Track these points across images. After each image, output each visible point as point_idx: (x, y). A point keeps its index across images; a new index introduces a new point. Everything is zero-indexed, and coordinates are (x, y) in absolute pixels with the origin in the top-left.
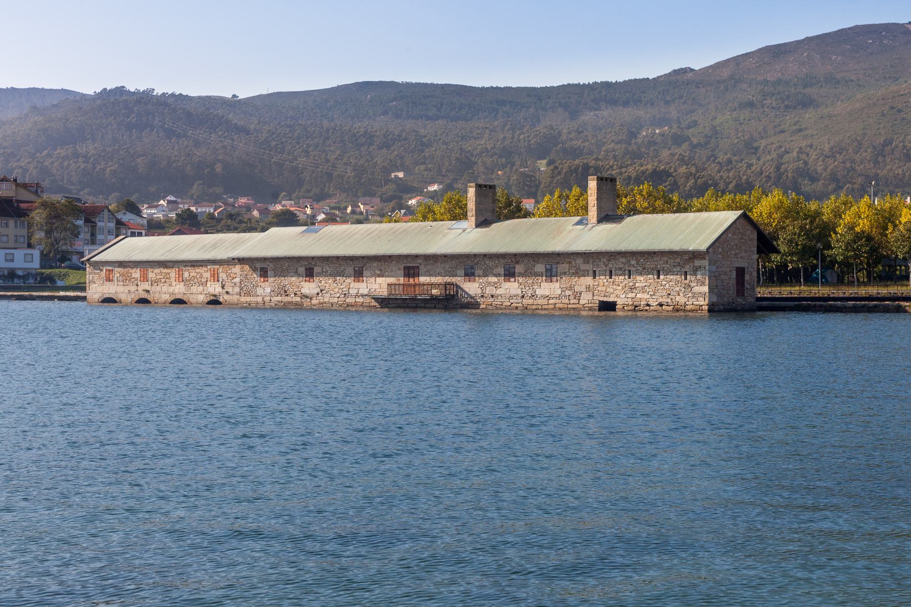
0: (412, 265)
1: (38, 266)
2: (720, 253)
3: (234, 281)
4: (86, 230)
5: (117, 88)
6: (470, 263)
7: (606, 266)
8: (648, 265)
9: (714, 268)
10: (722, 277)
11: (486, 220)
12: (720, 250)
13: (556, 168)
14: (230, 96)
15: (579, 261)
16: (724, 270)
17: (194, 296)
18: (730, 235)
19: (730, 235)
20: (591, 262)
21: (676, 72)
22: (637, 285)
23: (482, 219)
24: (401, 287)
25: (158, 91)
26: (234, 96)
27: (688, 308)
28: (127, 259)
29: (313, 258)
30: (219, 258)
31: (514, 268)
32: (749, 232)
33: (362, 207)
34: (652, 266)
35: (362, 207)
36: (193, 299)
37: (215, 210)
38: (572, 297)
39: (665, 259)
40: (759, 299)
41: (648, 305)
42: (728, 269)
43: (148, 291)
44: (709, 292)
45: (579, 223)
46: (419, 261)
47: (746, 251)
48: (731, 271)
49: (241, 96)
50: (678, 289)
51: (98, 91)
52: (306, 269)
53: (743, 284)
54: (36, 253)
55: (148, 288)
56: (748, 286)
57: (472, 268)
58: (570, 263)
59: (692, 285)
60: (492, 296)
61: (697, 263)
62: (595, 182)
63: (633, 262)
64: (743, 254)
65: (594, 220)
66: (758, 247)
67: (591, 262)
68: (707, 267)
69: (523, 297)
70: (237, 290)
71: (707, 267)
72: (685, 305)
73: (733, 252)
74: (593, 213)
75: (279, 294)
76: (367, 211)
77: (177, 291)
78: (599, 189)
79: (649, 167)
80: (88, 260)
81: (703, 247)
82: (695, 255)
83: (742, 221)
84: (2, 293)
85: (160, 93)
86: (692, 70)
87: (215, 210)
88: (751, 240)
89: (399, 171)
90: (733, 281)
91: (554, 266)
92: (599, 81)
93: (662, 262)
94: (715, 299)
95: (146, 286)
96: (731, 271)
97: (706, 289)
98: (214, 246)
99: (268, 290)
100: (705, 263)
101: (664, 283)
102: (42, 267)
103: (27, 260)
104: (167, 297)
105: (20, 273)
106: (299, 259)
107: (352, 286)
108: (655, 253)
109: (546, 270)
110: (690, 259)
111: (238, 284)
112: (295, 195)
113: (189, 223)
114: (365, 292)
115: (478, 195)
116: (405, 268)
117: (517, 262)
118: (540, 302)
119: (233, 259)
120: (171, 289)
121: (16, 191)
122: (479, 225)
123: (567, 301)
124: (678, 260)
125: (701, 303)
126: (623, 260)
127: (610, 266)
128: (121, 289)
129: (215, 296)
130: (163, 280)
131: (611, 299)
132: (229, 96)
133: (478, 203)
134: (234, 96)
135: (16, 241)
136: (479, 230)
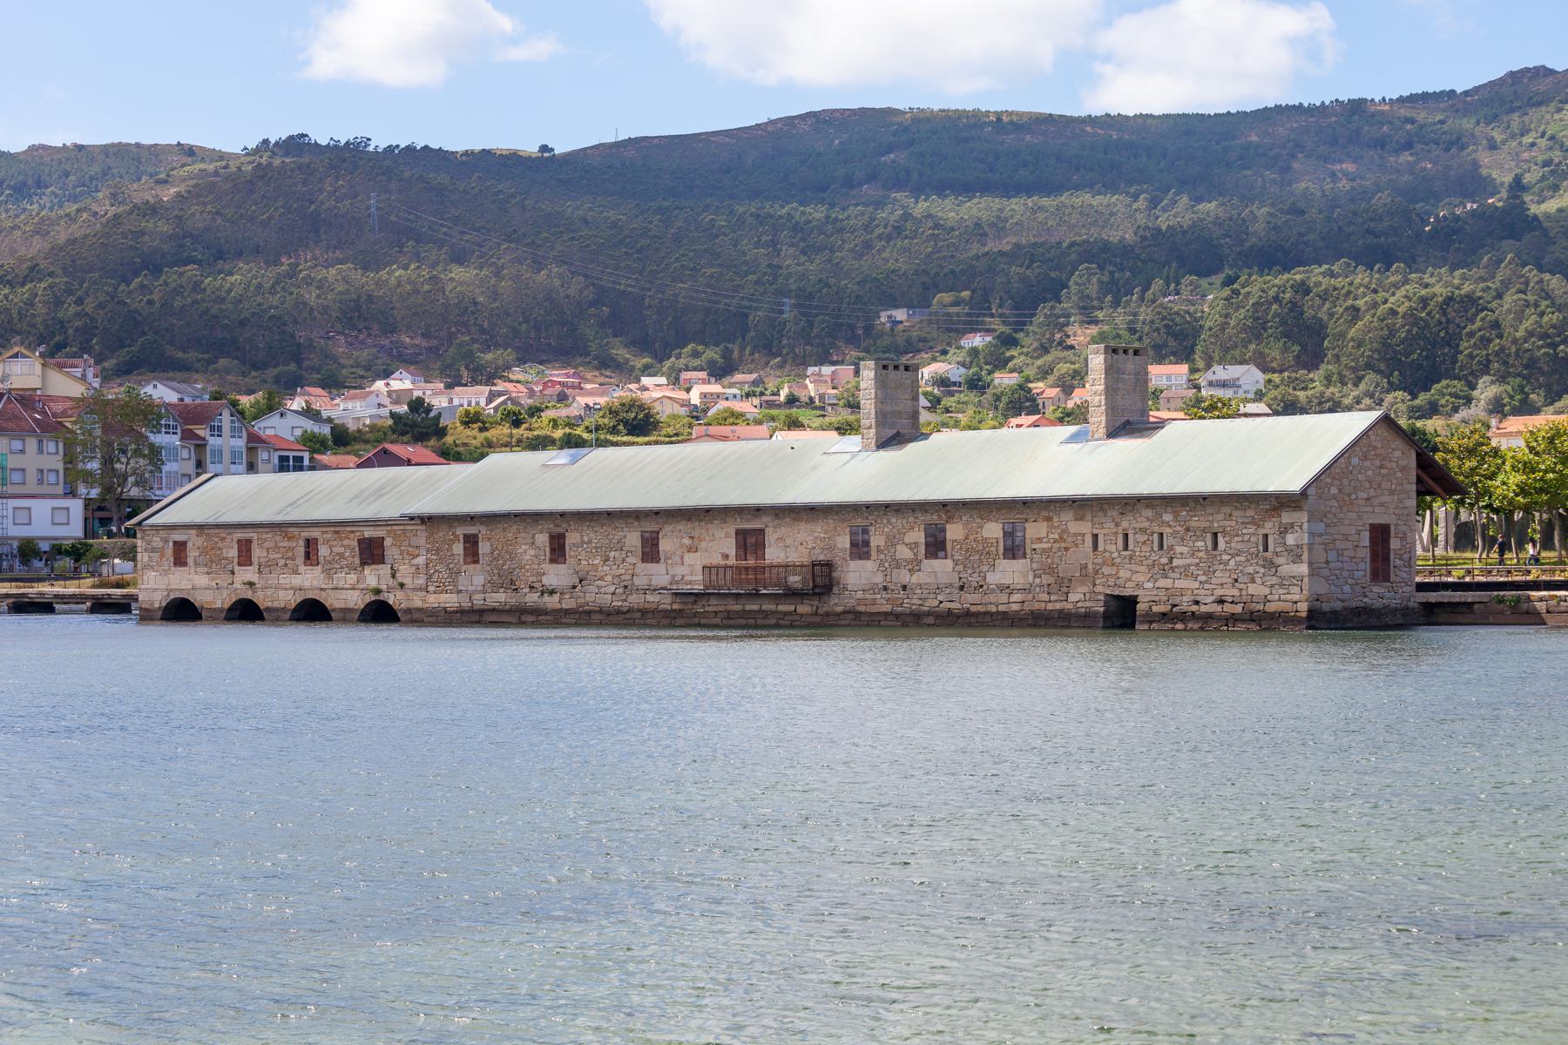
1: (79, 533)
3: (415, 561)
4: (185, 454)
5: (291, 138)
7: (1117, 525)
9: (1320, 527)
11: (898, 434)
12: (1334, 490)
13: (1236, 292)
14: (536, 149)
15: (1067, 516)
16: (1344, 530)
17: (343, 595)
18: (1355, 461)
19: (1355, 461)
20: (1089, 517)
21: (1514, 77)
22: (1176, 562)
24: (729, 573)
25: (379, 142)
26: (544, 148)
28: (211, 520)
29: (563, 514)
30: (386, 515)
31: (944, 530)
32: (1398, 454)
33: (811, 386)
35: (811, 386)
36: (332, 601)
38: (1055, 588)
39: (1227, 510)
40: (1421, 587)
41: (1197, 603)
43: (251, 584)
44: (1311, 575)
45: (1073, 439)
46: (765, 519)
47: (1392, 492)
48: (1358, 533)
49: (560, 148)
50: (1250, 570)
51: (252, 145)
52: (552, 538)
53: (1386, 559)
55: (254, 578)
56: (1398, 562)
57: (865, 531)
58: (1049, 519)
59: (1280, 560)
60: (904, 588)
61: (1287, 517)
62: (1101, 358)
65: (1102, 431)
66: (1419, 480)
67: (1089, 517)
68: (1305, 526)
69: (962, 588)
70: (421, 581)
71: (1305, 526)
72: (1267, 601)
73: (1364, 495)
74: (1098, 418)
75: (496, 587)
76: (822, 397)
77: (307, 584)
78: (1110, 370)
79: (1438, 289)
80: (140, 524)
81: (1295, 484)
82: (1280, 502)
83: (1384, 432)
84: (4, 591)
85: (383, 146)
86: (1552, 72)
87: (489, 401)
88: (1403, 469)
89: (897, 307)
91: (1019, 527)
92: (1344, 98)
93: (1220, 516)
94: (1322, 588)
95: (249, 574)
96: (1358, 533)
97: (1303, 569)
98: (379, 493)
99: (479, 580)
100: (1302, 517)
101: (1226, 557)
103: (55, 518)
104: (290, 599)
107: (638, 570)
109: (1005, 534)
110: (1274, 509)
112: (668, 364)
114: (663, 580)
116: (738, 532)
117: (950, 519)
118: (992, 598)
119: (412, 518)
120: (297, 580)
121: (44, 378)
123: (1045, 597)
124: (1250, 513)
125: (1296, 597)
126: (1149, 513)
127: (1125, 524)
128: (202, 580)
129: (378, 591)
130: (281, 562)
131: (1127, 592)
132: (531, 147)
133: (881, 401)
134: (544, 148)
135: (41, 482)
136: (882, 453)
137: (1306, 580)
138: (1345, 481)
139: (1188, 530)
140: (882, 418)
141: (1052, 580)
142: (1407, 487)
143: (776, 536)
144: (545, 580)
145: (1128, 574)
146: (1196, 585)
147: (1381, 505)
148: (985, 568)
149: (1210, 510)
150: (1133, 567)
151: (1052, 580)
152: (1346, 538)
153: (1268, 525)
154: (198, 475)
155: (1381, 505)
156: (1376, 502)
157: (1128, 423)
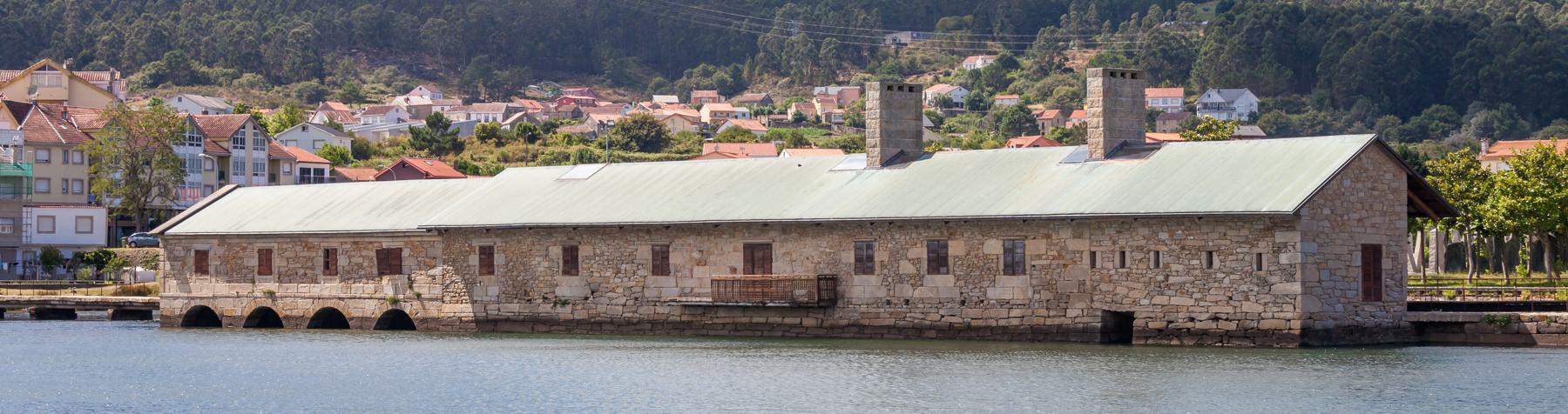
0: (757, 241)
2: (1327, 218)
6: (864, 237)
7: (1114, 243)
8: (1191, 241)
9: (1313, 247)
10: (1331, 264)
11: (902, 153)
12: (1327, 211)
15: (1065, 234)
16: (1338, 250)
17: (361, 304)
19: (1347, 183)
20: (1087, 235)
22: (1172, 280)
23: (896, 151)
27: (1265, 325)
28: (233, 230)
29: (576, 228)
31: (946, 247)
32: (1389, 176)
33: (818, 106)
34: (1198, 244)
35: (818, 106)
36: (352, 310)
37: (506, 117)
38: (1053, 304)
39: (1221, 229)
40: (1413, 307)
41: (1192, 320)
42: (1345, 250)
44: (1304, 294)
46: (772, 234)
47: (1383, 214)
50: (1245, 288)
52: (565, 250)
53: (1378, 278)
54: (100, 216)
56: (1390, 282)
57: (870, 247)
58: (1048, 237)
60: (907, 302)
61: (1280, 237)
63: (1164, 236)
64: (1377, 220)
66: (1410, 202)
67: (1087, 235)
68: (1298, 246)
69: (963, 303)
71: (1298, 246)
72: (1260, 318)
73: (1357, 216)
74: (1097, 137)
76: (828, 116)
78: (1107, 92)
80: (162, 233)
81: (1288, 205)
82: (1275, 222)
83: (1377, 156)
87: (506, 117)
88: (1394, 191)
90: (1357, 273)
93: (1216, 235)
94: (1315, 307)
97: (1296, 288)
98: (397, 205)
100: (1295, 237)
101: (1220, 275)
102: (769, 246)
105: (68, 254)
106: (549, 230)
108: (1200, 218)
110: (1268, 229)
111: (439, 280)
113: (439, 144)
115: (885, 103)
116: (746, 247)
117: (952, 235)
119: (429, 230)
121: (70, 89)
122: (887, 162)
123: (1044, 312)
124: (1245, 232)
125: (1289, 315)
126: (1145, 231)
127: (1122, 242)
130: (301, 272)
133: (885, 120)
135: (65, 191)
136: (886, 171)
137: (1299, 298)
138: (1338, 203)
139: (1183, 248)
140: (887, 137)
141: (1051, 296)
142: (1398, 208)
143: (783, 250)
144: (558, 291)
145: (1125, 291)
146: (1192, 302)
147: (1373, 226)
148: (986, 284)
149: (1205, 229)
150: (1130, 284)
151: (1051, 296)
152: (1338, 257)
153: (1262, 244)
154: (221, 186)
155: (1373, 226)
156: (1367, 223)
157: (1125, 144)
